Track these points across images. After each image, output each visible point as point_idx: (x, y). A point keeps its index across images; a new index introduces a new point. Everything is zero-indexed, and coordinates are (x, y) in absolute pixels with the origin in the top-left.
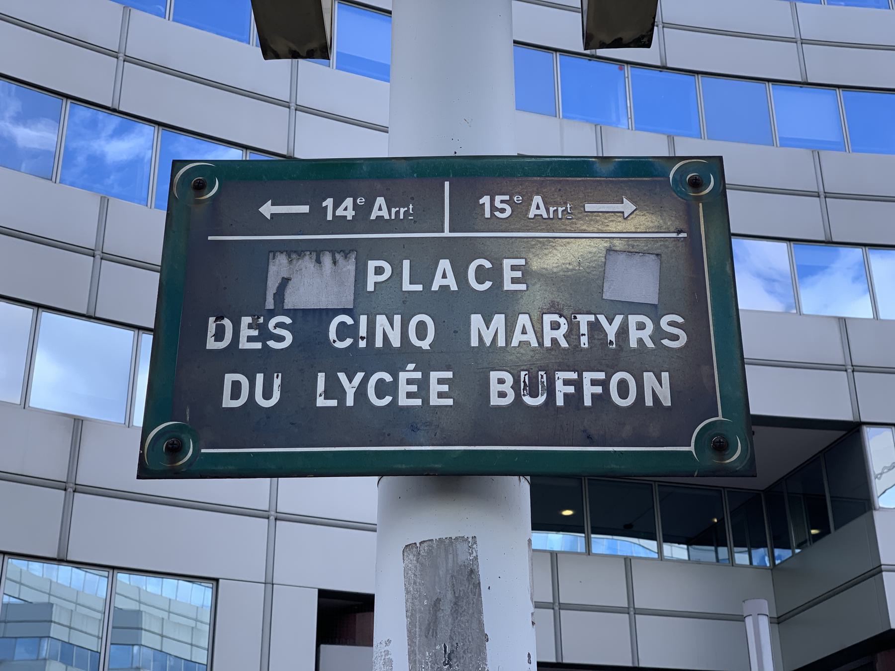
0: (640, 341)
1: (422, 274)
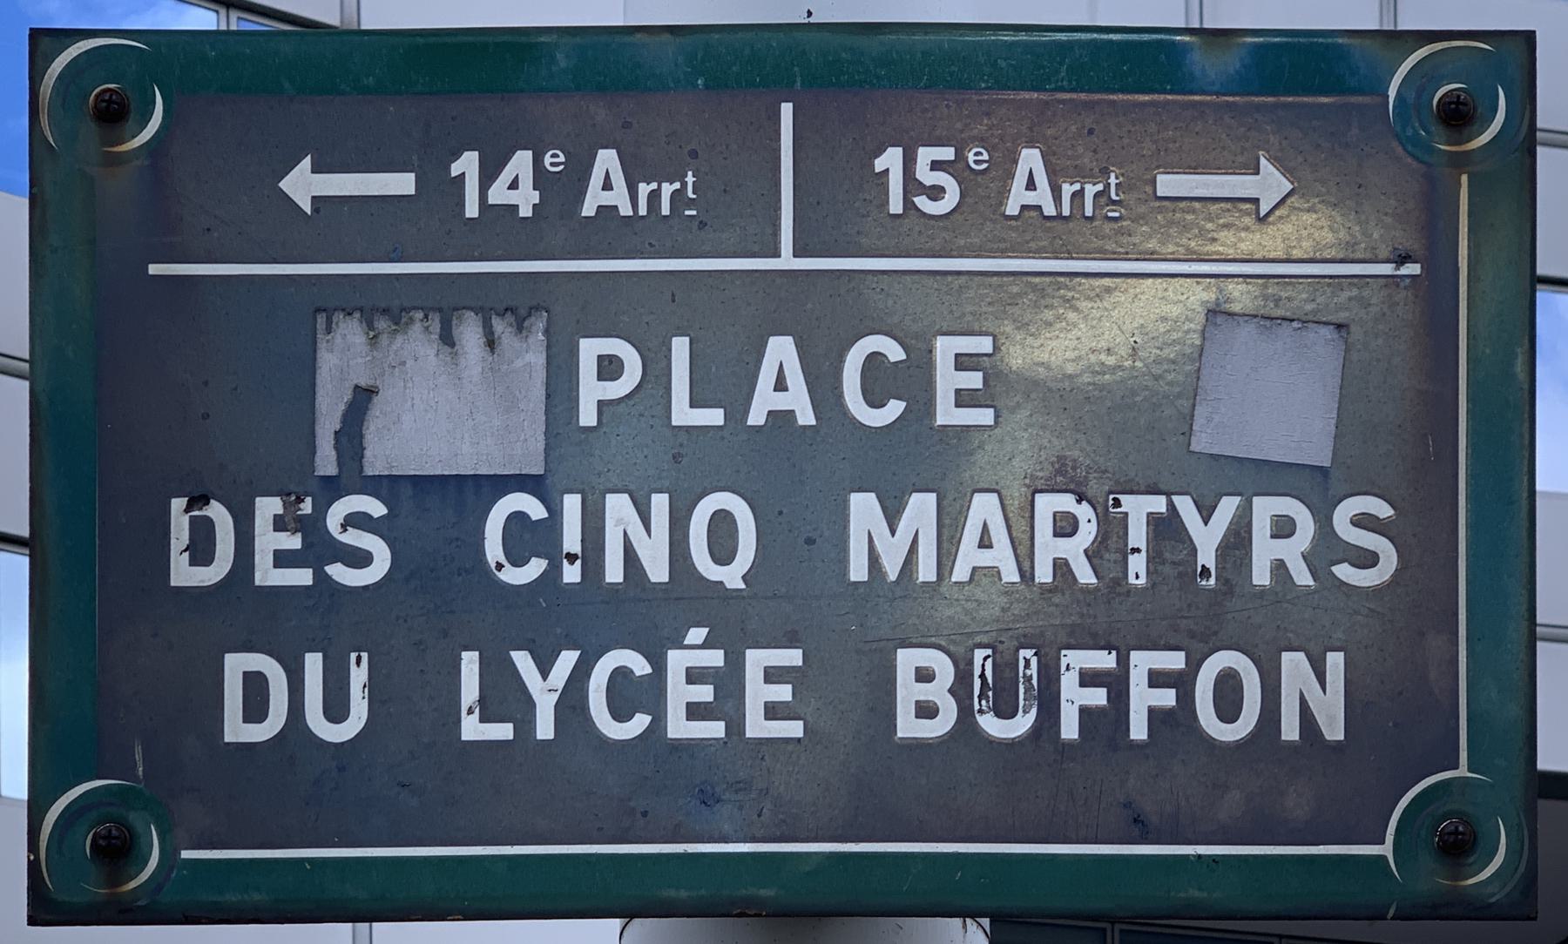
0: (1279, 567)
1: (725, 380)
